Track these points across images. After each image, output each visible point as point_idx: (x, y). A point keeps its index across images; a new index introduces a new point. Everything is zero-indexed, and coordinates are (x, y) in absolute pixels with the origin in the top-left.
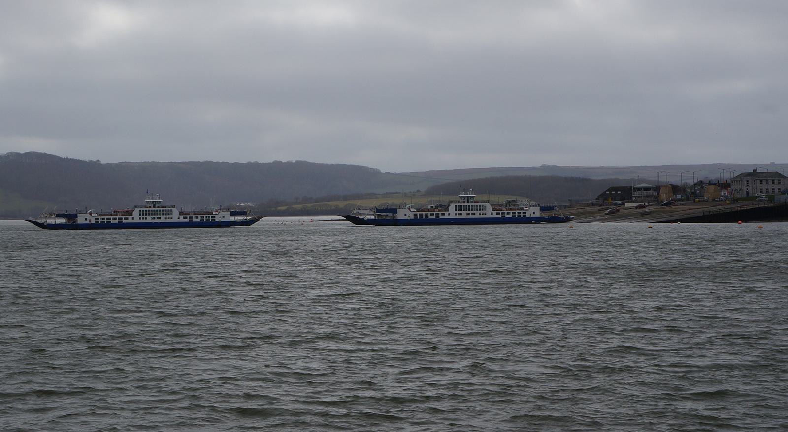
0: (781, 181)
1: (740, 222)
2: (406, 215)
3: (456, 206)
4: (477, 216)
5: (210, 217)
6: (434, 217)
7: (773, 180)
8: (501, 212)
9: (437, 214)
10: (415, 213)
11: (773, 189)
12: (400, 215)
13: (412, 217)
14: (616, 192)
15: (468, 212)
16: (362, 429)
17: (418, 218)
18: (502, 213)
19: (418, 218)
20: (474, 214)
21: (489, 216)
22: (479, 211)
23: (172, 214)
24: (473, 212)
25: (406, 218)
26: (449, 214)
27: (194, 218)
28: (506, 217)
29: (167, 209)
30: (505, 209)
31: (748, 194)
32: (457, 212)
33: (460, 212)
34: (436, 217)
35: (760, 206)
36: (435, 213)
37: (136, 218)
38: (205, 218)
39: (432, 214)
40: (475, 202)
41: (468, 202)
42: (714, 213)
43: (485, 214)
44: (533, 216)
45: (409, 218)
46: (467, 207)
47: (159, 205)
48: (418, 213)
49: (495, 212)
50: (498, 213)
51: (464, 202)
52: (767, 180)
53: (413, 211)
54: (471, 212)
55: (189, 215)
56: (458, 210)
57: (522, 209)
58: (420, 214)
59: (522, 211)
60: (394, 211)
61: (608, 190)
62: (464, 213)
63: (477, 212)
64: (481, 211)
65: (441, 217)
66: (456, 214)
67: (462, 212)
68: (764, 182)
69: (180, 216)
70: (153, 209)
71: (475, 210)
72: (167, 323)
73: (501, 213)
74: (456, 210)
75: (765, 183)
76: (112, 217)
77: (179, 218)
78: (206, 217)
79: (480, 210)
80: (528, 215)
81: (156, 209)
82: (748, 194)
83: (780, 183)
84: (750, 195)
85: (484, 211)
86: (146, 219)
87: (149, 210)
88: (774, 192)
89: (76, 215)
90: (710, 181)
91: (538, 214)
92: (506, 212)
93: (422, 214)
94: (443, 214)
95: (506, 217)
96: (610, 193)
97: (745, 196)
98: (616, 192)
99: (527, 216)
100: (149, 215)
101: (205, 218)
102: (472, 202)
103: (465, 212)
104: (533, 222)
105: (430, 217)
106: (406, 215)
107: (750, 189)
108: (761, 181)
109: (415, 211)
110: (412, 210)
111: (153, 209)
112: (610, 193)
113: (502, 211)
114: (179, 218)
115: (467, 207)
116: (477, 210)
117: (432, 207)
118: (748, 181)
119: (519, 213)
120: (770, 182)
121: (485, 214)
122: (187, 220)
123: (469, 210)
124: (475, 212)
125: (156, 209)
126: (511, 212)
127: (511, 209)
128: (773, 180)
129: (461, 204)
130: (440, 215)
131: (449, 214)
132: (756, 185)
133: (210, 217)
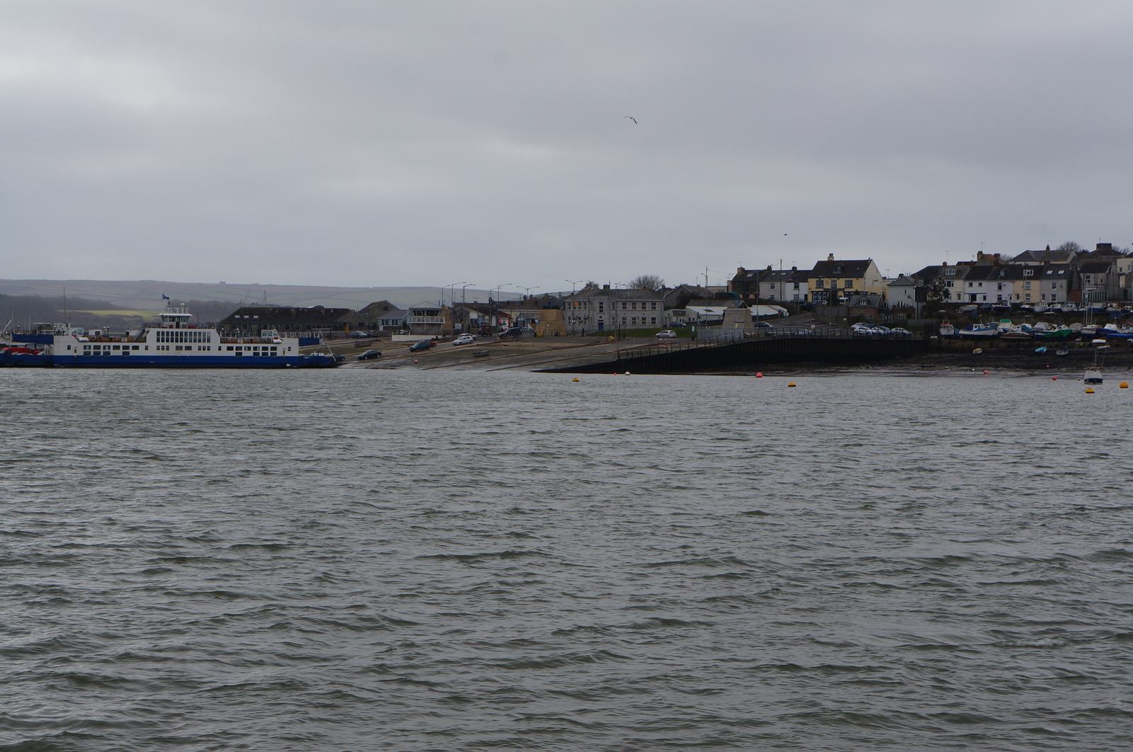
0: (657, 306)
1: (759, 374)
2: (69, 348)
3: (158, 333)
4: (195, 352)
5: (92, 347)
6: (119, 353)
7: (644, 304)
8: (234, 346)
9: (125, 348)
10: (86, 344)
11: (644, 319)
12: (60, 348)
13: (81, 352)
14: (251, 316)
15: (179, 344)
16: (520, 750)
17: (92, 354)
18: (237, 348)
19: (92, 354)
20: (189, 348)
21: (214, 352)
22: (198, 344)
23: (209, 341)
24: (188, 344)
25: (70, 353)
26: (147, 349)
27: (131, 348)
28: (131, 354)
29: (198, 330)
30: (242, 341)
31: (601, 325)
32: (161, 344)
33: (165, 344)
34: (123, 352)
35: (699, 346)
36: (121, 345)
37: (151, 347)
38: (102, 348)
39: (116, 348)
40: (190, 327)
41: (178, 326)
42: (634, 357)
43: (209, 349)
44: (288, 354)
45: (75, 354)
46: (204, 335)
47: (185, 323)
48: (92, 344)
49: (224, 346)
50: (230, 349)
51: (171, 327)
52: (634, 304)
53: (83, 341)
54: (184, 344)
55: (237, 343)
56: (163, 341)
57: (269, 341)
58: (96, 347)
59: (269, 346)
60: (49, 340)
61: (238, 312)
62: (173, 345)
63: (195, 346)
64: (202, 344)
65: (133, 353)
66: (158, 349)
67: (169, 344)
68: (629, 306)
69: (221, 345)
70: (175, 330)
71: (191, 341)
72: (1008, 564)
73: (121, 348)
74: (158, 340)
75: (631, 308)
76: (112, 344)
77: (220, 349)
78: (104, 347)
79: (200, 341)
80: (279, 353)
81: (179, 330)
82: (601, 325)
83: (655, 308)
84: (606, 328)
85: (206, 344)
86: (168, 349)
87: (168, 333)
88: (654, 323)
89: (52, 337)
90: (550, 303)
91: (295, 352)
92: (244, 346)
93: (99, 347)
94: (136, 348)
95: (131, 354)
96: (242, 318)
97: (596, 328)
98: (251, 316)
99: (278, 355)
100: (172, 341)
101: (102, 348)
102: (184, 327)
103: (175, 344)
104: (288, 365)
105: (114, 353)
106: (69, 348)
107: (605, 317)
108: (624, 304)
109: (85, 341)
110: (81, 339)
111: (175, 330)
112: (242, 318)
113: (238, 345)
114: (220, 349)
115: (204, 335)
116: (195, 341)
117: (97, 333)
118: (601, 303)
119: (264, 348)
120: (639, 306)
121: (209, 349)
122: (233, 353)
123: (181, 341)
124: (192, 344)
125: (179, 330)
126: (252, 346)
127: (252, 342)
128: (644, 304)
129: (163, 330)
130: (243, 351)
131: (147, 349)
132: (616, 311)
133: (92, 347)
